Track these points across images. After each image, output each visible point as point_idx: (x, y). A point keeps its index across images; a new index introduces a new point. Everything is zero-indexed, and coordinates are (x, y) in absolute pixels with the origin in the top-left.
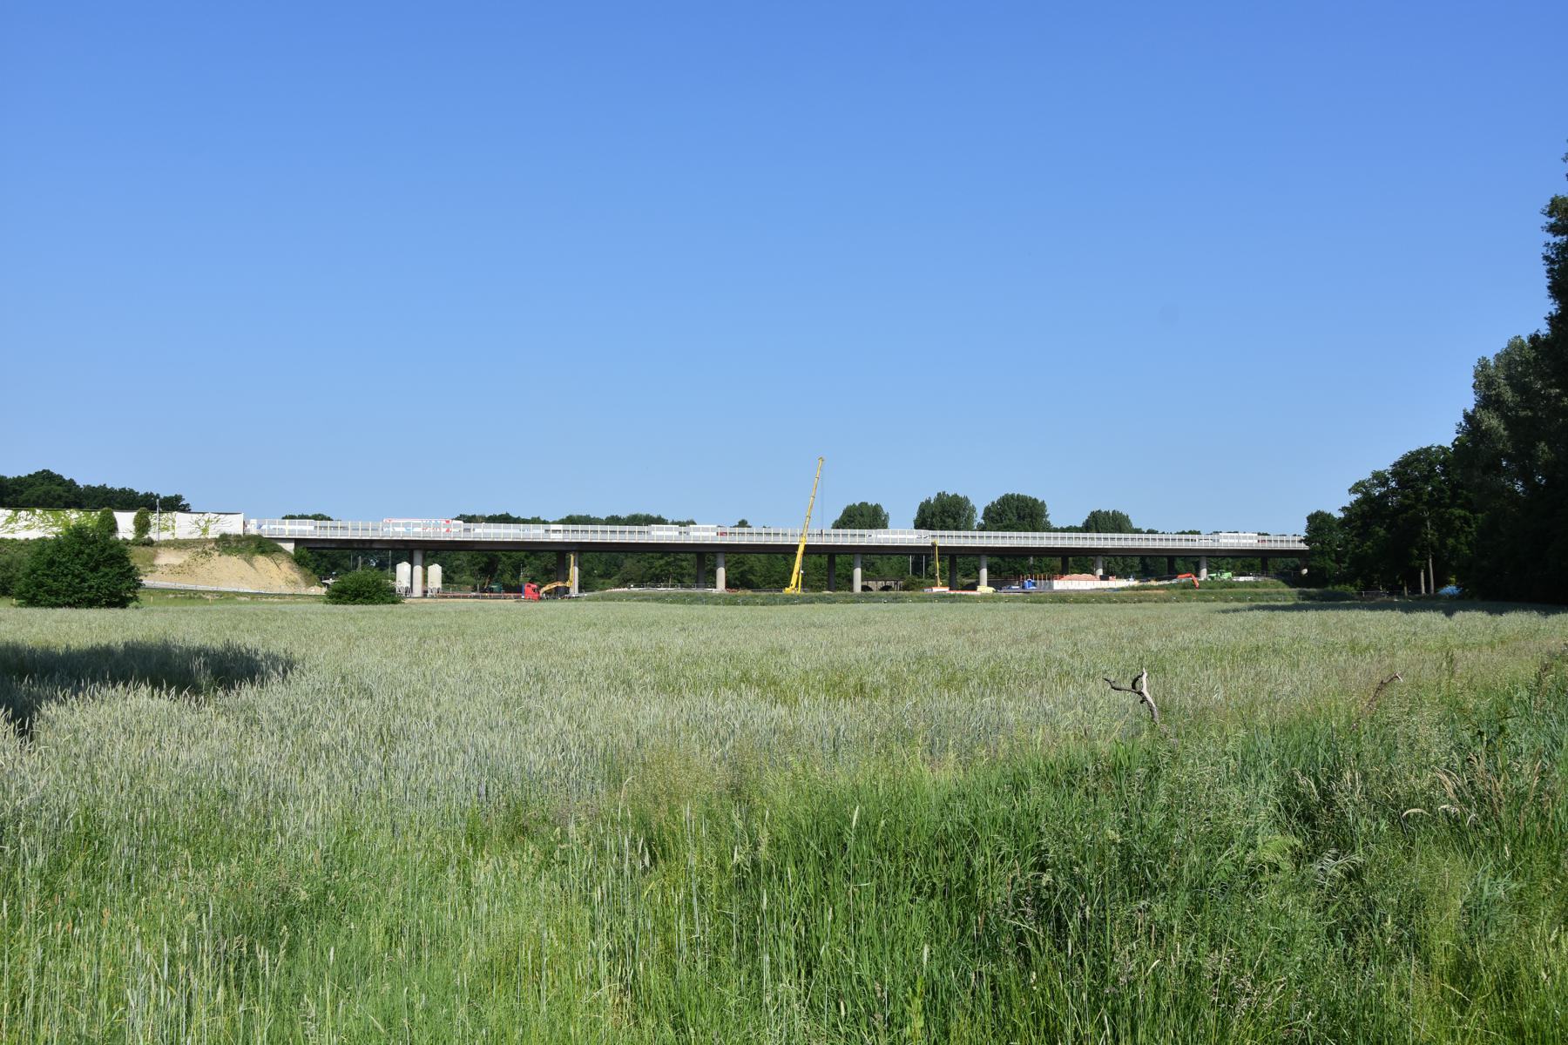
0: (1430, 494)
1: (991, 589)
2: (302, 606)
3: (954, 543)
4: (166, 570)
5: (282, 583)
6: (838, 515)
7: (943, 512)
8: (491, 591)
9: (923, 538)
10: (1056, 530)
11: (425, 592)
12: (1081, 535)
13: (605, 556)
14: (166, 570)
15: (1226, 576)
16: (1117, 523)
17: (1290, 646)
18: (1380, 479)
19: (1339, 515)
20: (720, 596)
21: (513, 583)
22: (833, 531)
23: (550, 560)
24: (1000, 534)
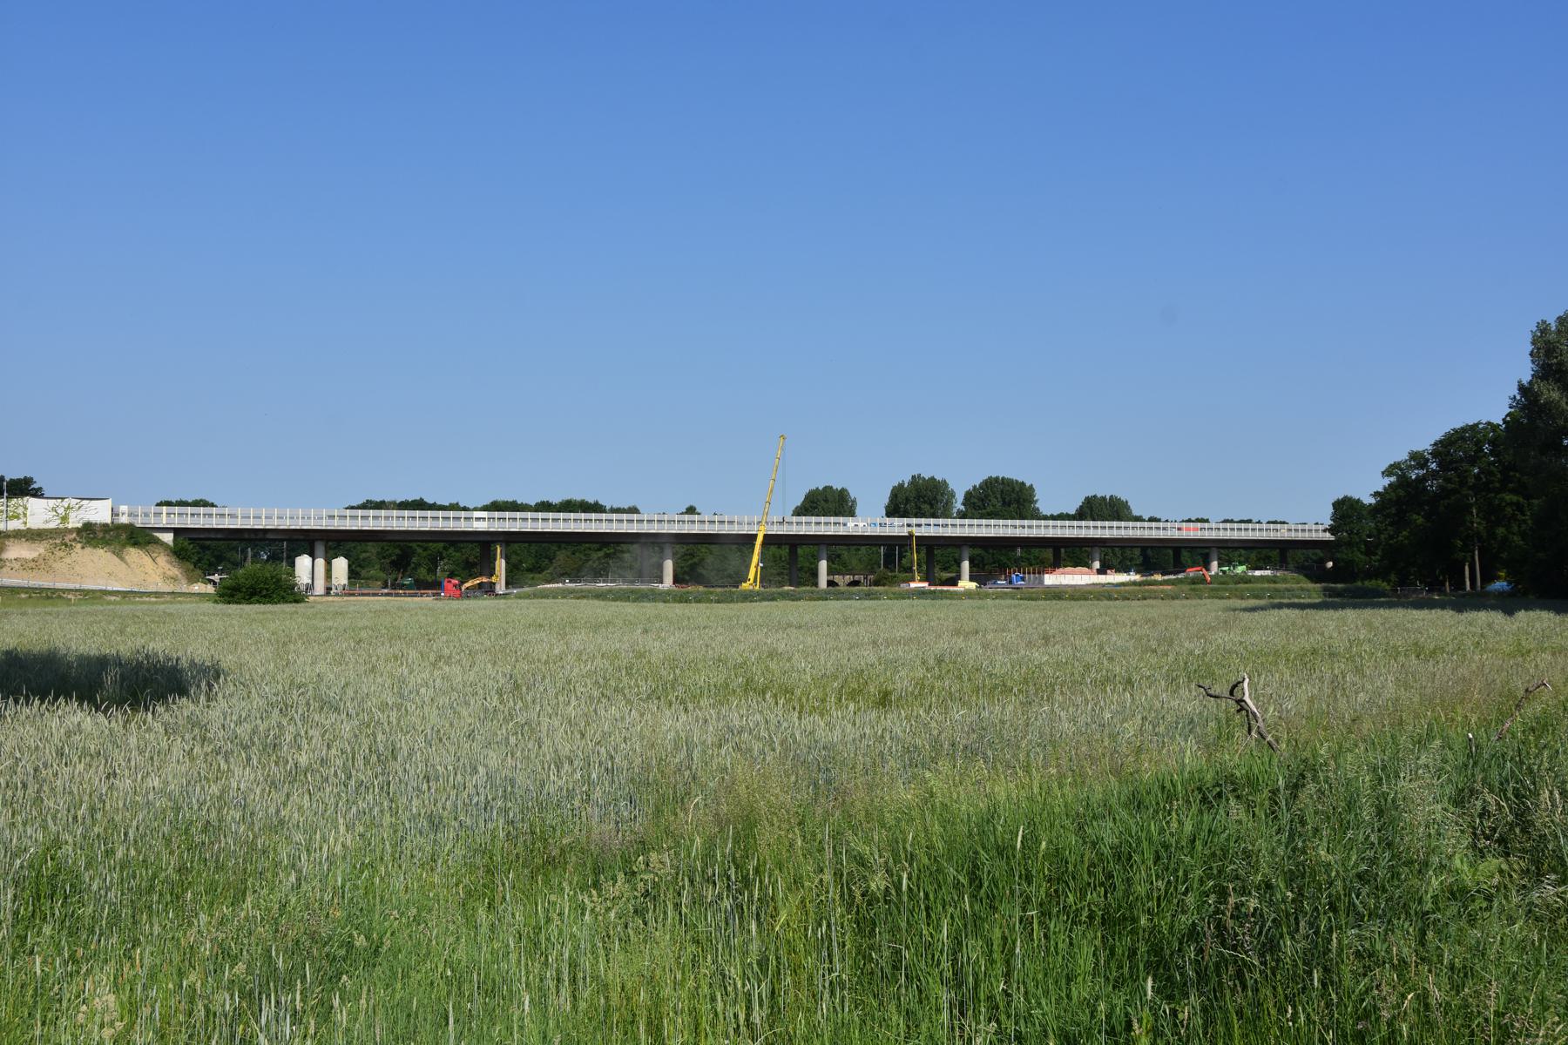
0: (1477, 477)
1: (973, 585)
2: (189, 607)
3: (932, 532)
4: (16, 565)
5: (158, 580)
6: (799, 500)
7: (918, 497)
8: (402, 587)
9: (898, 527)
10: (1045, 518)
11: (328, 589)
12: (1075, 523)
13: (534, 548)
14: (16, 565)
15: (1240, 569)
16: (1114, 509)
17: (1349, 650)
18: (1418, 459)
19: (1369, 500)
20: (668, 593)
21: (430, 578)
22: (795, 519)
23: (473, 553)
24: (984, 522)
